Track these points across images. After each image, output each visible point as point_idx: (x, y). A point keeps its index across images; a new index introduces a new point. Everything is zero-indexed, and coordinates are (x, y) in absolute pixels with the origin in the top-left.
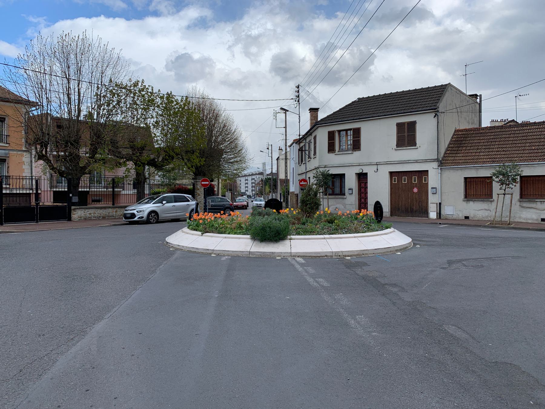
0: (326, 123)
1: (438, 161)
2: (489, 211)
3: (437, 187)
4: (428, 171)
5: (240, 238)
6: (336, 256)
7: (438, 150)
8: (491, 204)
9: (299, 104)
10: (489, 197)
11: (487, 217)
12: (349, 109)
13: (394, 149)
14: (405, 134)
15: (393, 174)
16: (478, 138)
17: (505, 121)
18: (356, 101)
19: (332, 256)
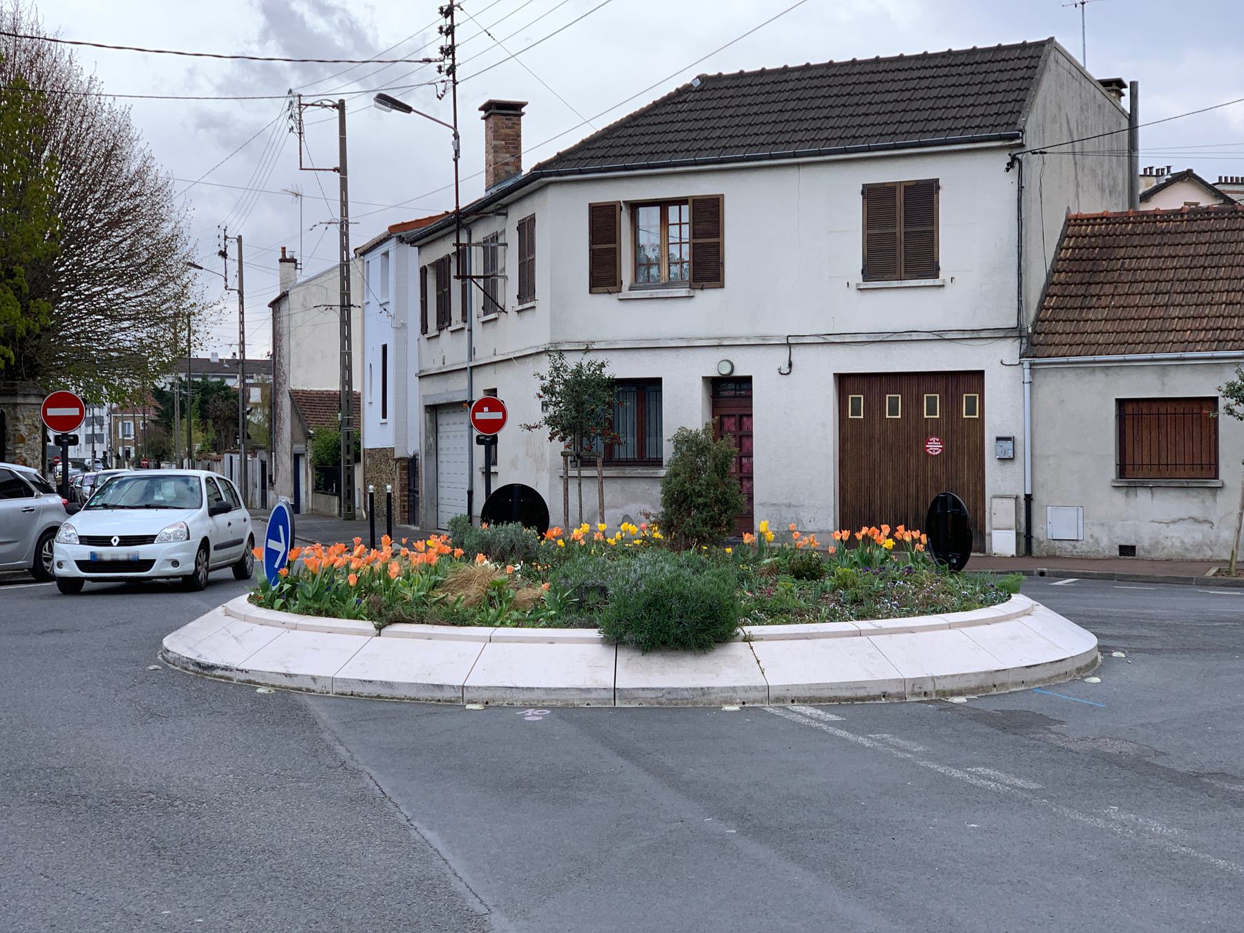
0: (581, 172)
1: (1021, 337)
2: (1206, 527)
3: (1019, 438)
4: (981, 373)
5: (911, 630)
6: (914, 694)
7: (1020, 293)
8: (1215, 501)
9: (455, 83)
10: (1205, 474)
11: (1199, 547)
12: (670, 118)
13: (853, 284)
14: (898, 229)
15: (849, 383)
16: (1155, 252)
17: (1160, 173)
18: (691, 85)
19: (901, 696)
